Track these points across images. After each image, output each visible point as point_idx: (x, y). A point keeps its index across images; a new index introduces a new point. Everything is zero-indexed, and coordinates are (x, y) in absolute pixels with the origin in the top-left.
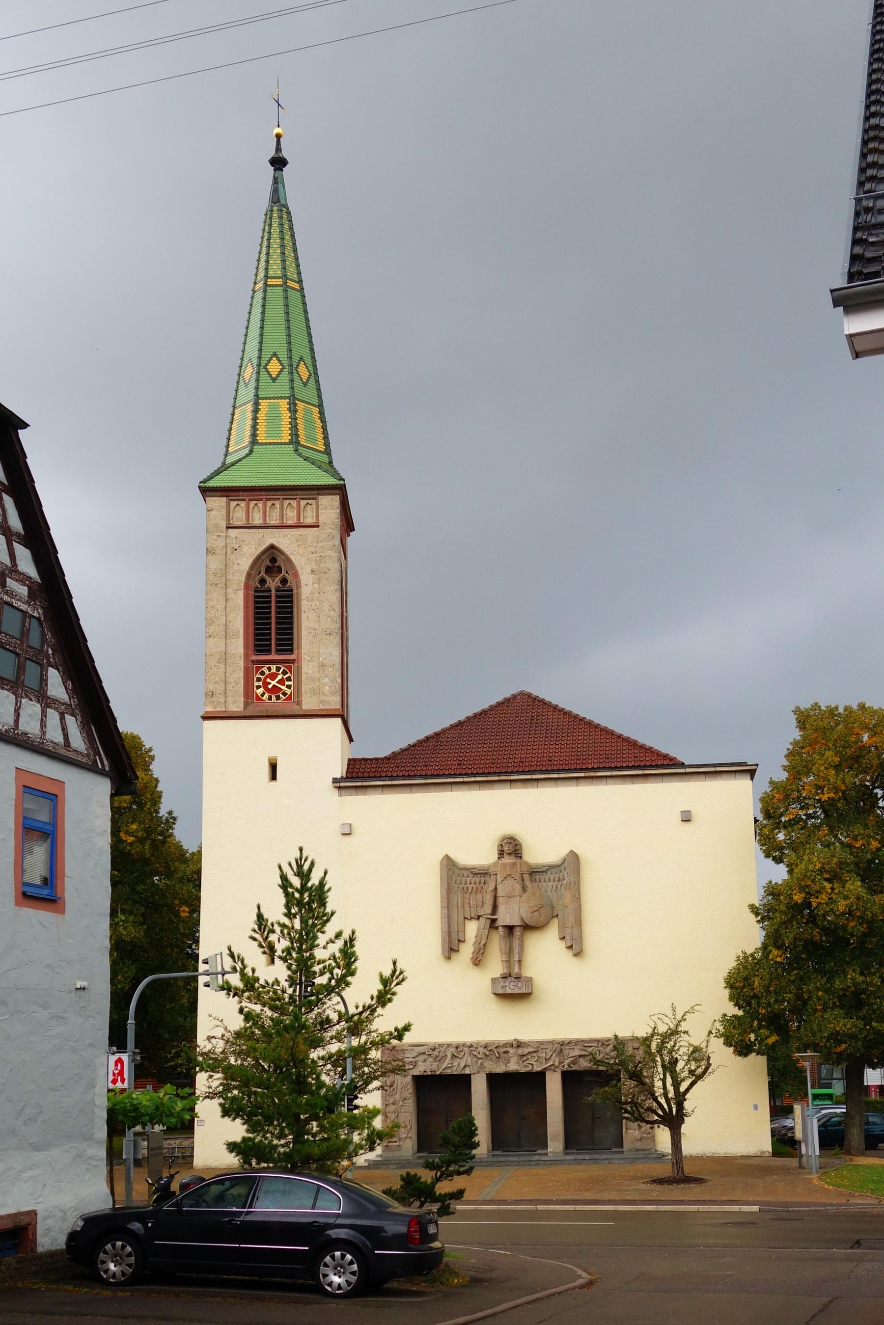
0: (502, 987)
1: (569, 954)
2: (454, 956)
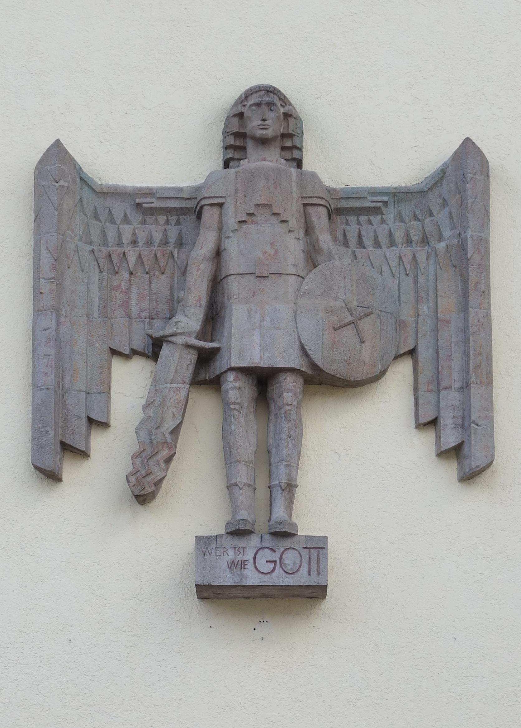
0: (232, 565)
1: (449, 470)
2: (71, 471)
